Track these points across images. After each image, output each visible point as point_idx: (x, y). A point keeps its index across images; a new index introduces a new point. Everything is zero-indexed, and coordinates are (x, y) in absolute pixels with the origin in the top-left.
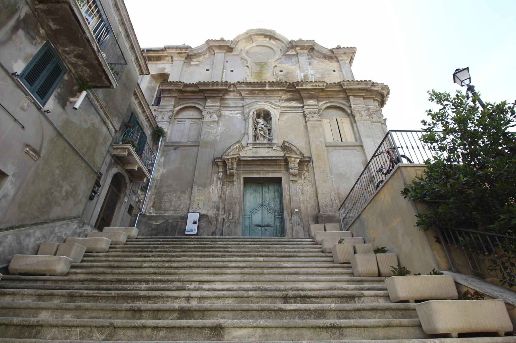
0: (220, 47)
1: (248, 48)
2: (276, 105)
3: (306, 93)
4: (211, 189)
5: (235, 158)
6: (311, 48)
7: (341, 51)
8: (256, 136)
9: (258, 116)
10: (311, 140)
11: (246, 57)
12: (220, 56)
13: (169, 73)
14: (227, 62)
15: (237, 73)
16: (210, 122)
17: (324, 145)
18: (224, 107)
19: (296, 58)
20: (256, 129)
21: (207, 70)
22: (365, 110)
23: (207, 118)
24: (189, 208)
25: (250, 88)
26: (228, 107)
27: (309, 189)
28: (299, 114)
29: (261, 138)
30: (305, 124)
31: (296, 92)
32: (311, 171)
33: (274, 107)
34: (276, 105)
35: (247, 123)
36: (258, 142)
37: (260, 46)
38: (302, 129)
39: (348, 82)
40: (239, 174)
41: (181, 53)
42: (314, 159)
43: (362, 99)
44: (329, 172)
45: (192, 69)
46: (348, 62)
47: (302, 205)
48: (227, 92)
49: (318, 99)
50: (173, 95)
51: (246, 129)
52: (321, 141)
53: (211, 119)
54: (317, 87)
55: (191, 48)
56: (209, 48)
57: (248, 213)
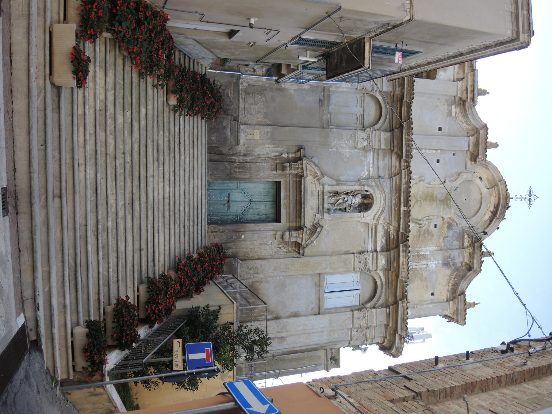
2: (379, 218)
3: (394, 256)
4: (268, 146)
5: (303, 172)
7: (461, 306)
8: (337, 194)
9: (365, 197)
10: (328, 257)
11: (460, 180)
12: (465, 144)
13: (438, 77)
14: (454, 154)
15: (427, 171)
16: (356, 139)
17: (321, 272)
21: (440, 129)
22: (367, 324)
25: (403, 187)
26: (378, 159)
27: (266, 251)
28: (366, 246)
29: (333, 200)
30: (351, 252)
31: (396, 244)
32: (289, 255)
34: (379, 218)
35: (353, 183)
36: (326, 197)
37: (482, 198)
38: (344, 249)
39: (406, 307)
40: (286, 176)
42: (303, 259)
47: (249, 243)
49: (387, 270)
50: (397, 89)
53: (359, 139)
54: (401, 270)
55: (474, 106)
56: (477, 129)
57: (243, 185)
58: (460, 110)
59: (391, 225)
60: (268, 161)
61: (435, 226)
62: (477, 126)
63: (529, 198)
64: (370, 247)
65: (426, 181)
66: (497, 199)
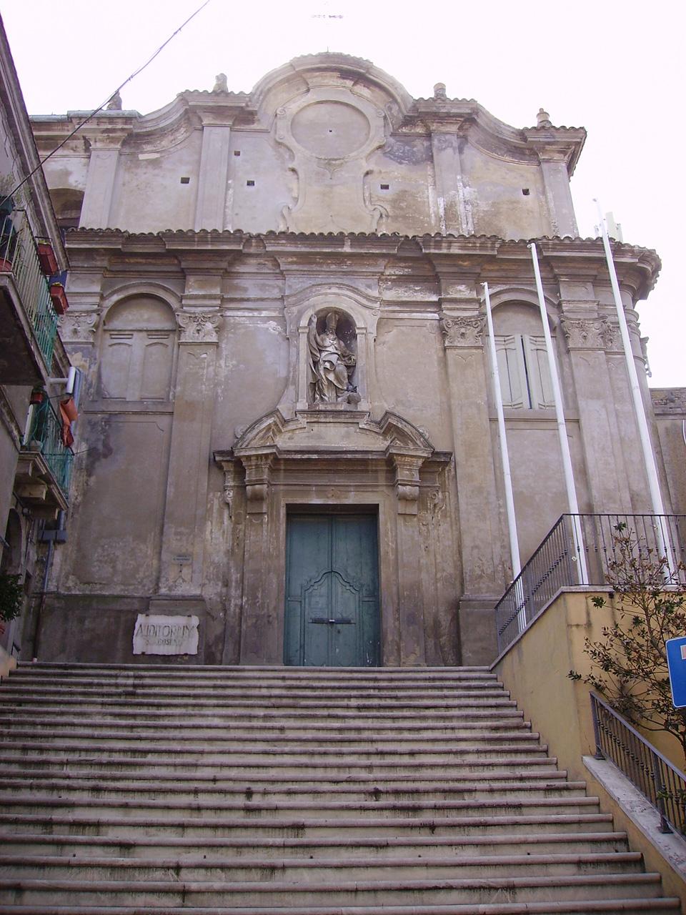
0: (218, 111)
1: (294, 107)
2: (367, 297)
3: (449, 266)
5: (266, 456)
8: (315, 386)
11: (290, 141)
12: (217, 136)
13: (80, 187)
14: (237, 154)
18: (232, 300)
20: (316, 363)
21: (185, 181)
23: (189, 335)
24: (158, 579)
26: (242, 300)
28: (428, 323)
29: (329, 394)
30: (441, 354)
31: (423, 261)
33: (364, 301)
34: (367, 297)
35: (293, 350)
36: (322, 407)
38: (435, 368)
41: (114, 130)
42: (460, 456)
43: (590, 286)
44: (493, 490)
45: (144, 175)
46: (563, 166)
48: (239, 256)
50: (99, 264)
51: (292, 367)
52: (478, 407)
55: (141, 117)
56: (186, 112)
58: (148, 143)
60: (242, 533)
62: (182, 111)
64: (430, 316)
66: (329, 74)
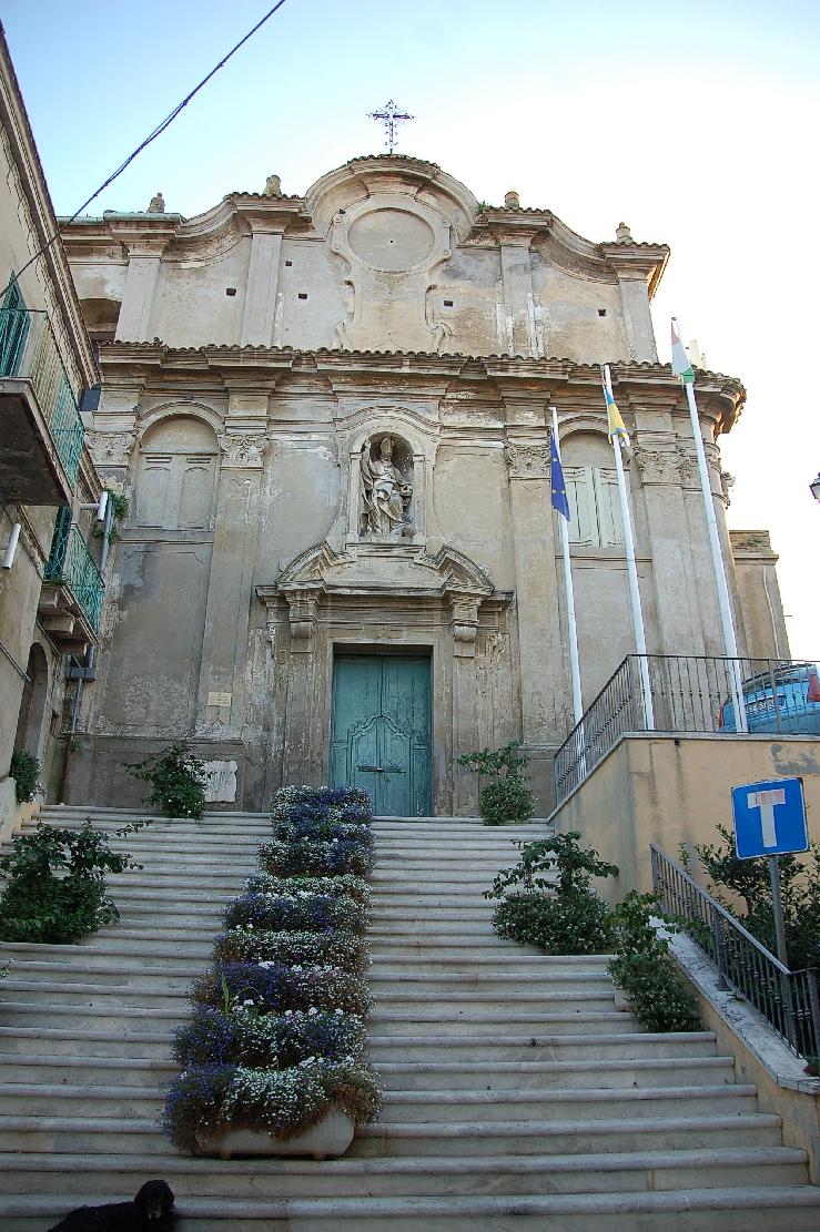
2: (426, 422)
5: (312, 591)
6: (541, 231)
8: (368, 517)
9: (376, 453)
11: (347, 251)
13: (115, 298)
14: (289, 264)
19: (496, 258)
20: (368, 493)
21: (231, 292)
33: (423, 427)
34: (426, 422)
42: (522, 596)
43: (668, 416)
45: (186, 285)
48: (287, 376)
53: (244, 463)
55: (185, 221)
59: (443, 397)
61: (449, 304)
63: (391, 119)
65: (345, 322)
